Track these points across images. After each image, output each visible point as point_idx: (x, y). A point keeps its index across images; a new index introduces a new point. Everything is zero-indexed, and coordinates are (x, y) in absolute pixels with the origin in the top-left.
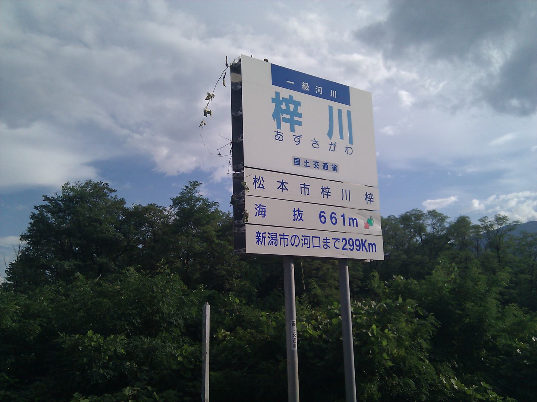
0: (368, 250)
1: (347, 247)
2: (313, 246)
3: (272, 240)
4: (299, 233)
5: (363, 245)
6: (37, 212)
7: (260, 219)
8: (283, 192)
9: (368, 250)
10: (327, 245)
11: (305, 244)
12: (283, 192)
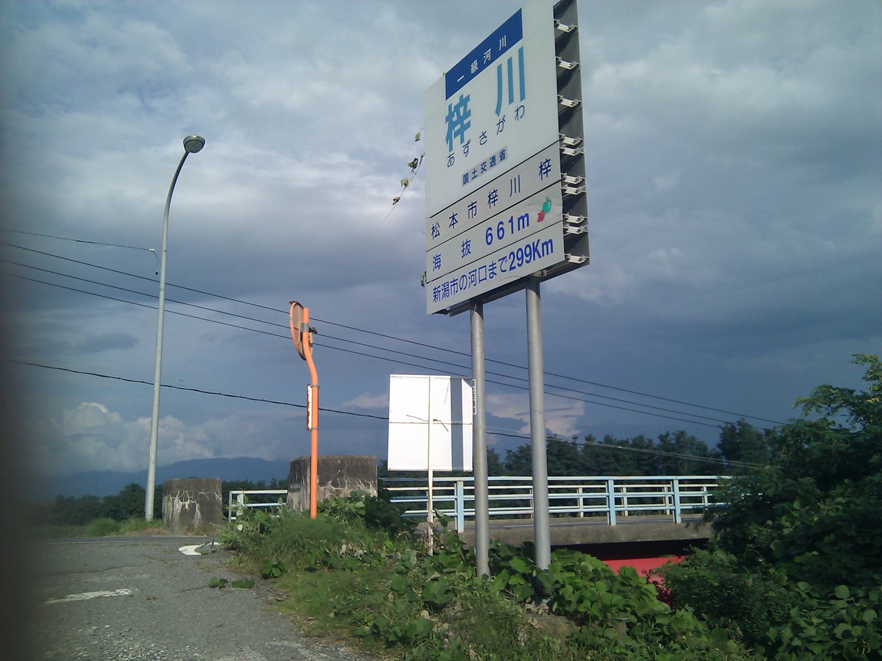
0: (541, 255)
1: (516, 262)
2: (480, 281)
3: (445, 291)
4: (449, 278)
5: (536, 250)
6: (685, 434)
7: (438, 272)
8: (457, 214)
9: (541, 255)
10: (493, 273)
11: (472, 282)
12: (457, 214)
